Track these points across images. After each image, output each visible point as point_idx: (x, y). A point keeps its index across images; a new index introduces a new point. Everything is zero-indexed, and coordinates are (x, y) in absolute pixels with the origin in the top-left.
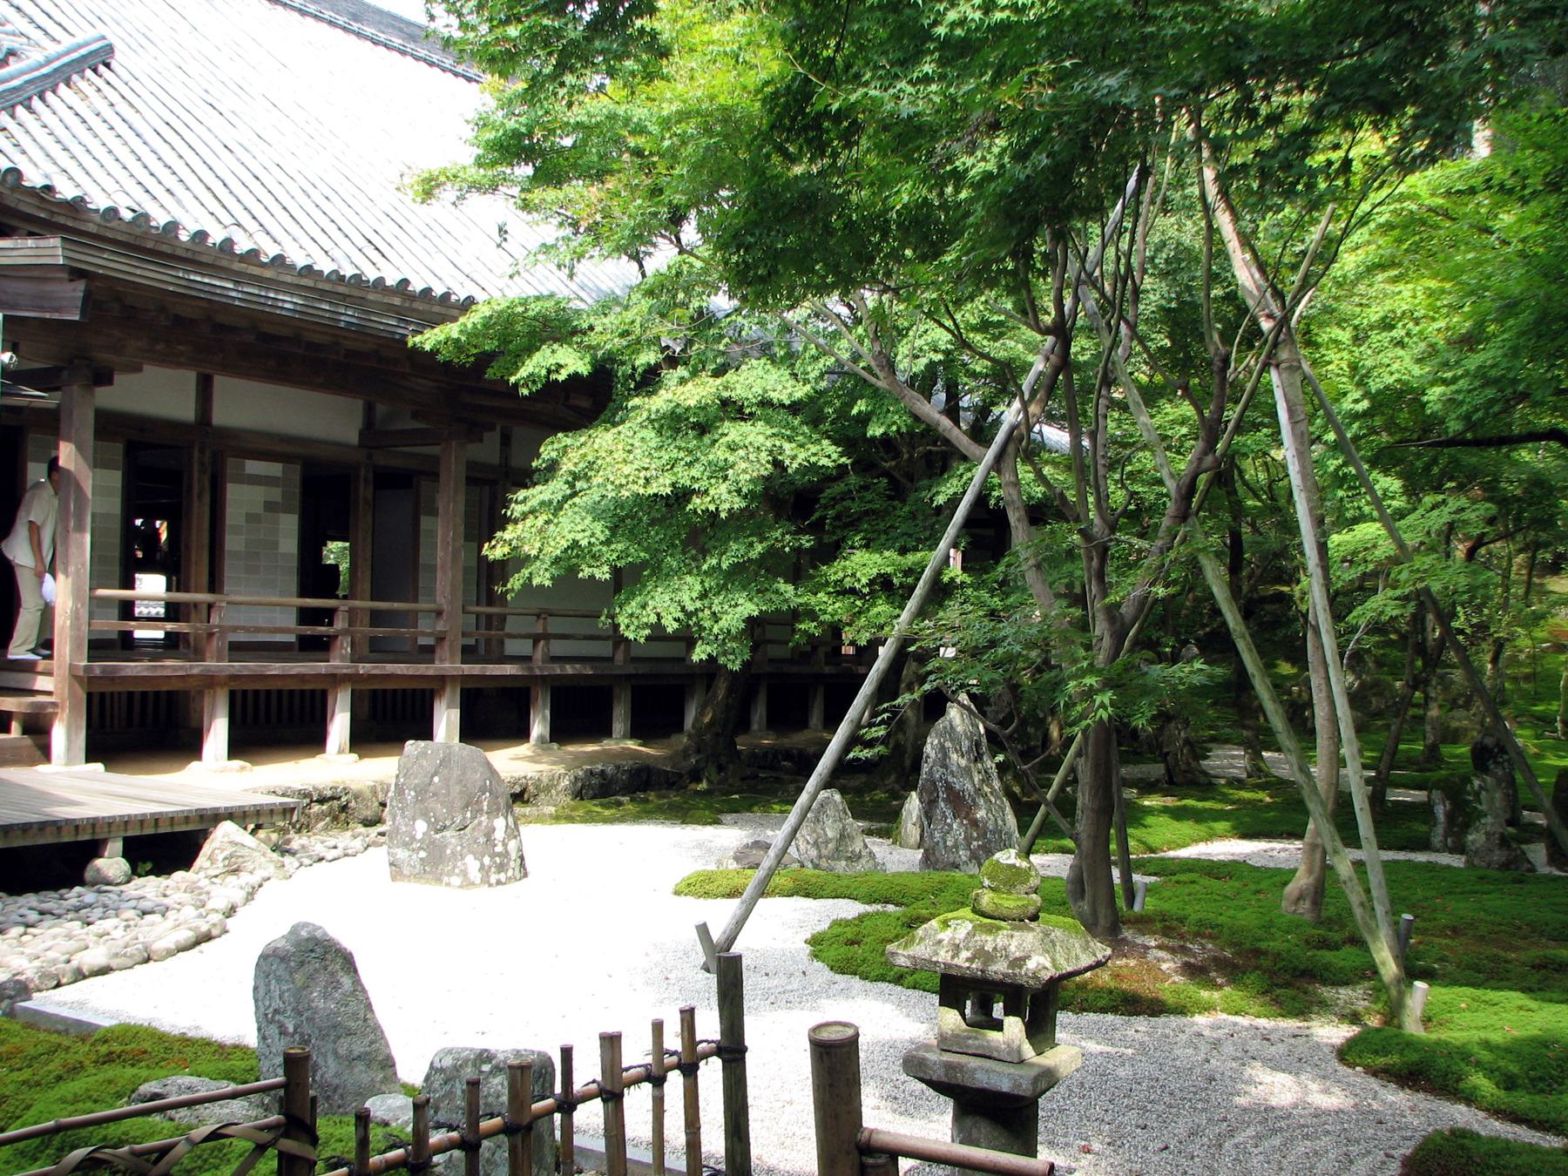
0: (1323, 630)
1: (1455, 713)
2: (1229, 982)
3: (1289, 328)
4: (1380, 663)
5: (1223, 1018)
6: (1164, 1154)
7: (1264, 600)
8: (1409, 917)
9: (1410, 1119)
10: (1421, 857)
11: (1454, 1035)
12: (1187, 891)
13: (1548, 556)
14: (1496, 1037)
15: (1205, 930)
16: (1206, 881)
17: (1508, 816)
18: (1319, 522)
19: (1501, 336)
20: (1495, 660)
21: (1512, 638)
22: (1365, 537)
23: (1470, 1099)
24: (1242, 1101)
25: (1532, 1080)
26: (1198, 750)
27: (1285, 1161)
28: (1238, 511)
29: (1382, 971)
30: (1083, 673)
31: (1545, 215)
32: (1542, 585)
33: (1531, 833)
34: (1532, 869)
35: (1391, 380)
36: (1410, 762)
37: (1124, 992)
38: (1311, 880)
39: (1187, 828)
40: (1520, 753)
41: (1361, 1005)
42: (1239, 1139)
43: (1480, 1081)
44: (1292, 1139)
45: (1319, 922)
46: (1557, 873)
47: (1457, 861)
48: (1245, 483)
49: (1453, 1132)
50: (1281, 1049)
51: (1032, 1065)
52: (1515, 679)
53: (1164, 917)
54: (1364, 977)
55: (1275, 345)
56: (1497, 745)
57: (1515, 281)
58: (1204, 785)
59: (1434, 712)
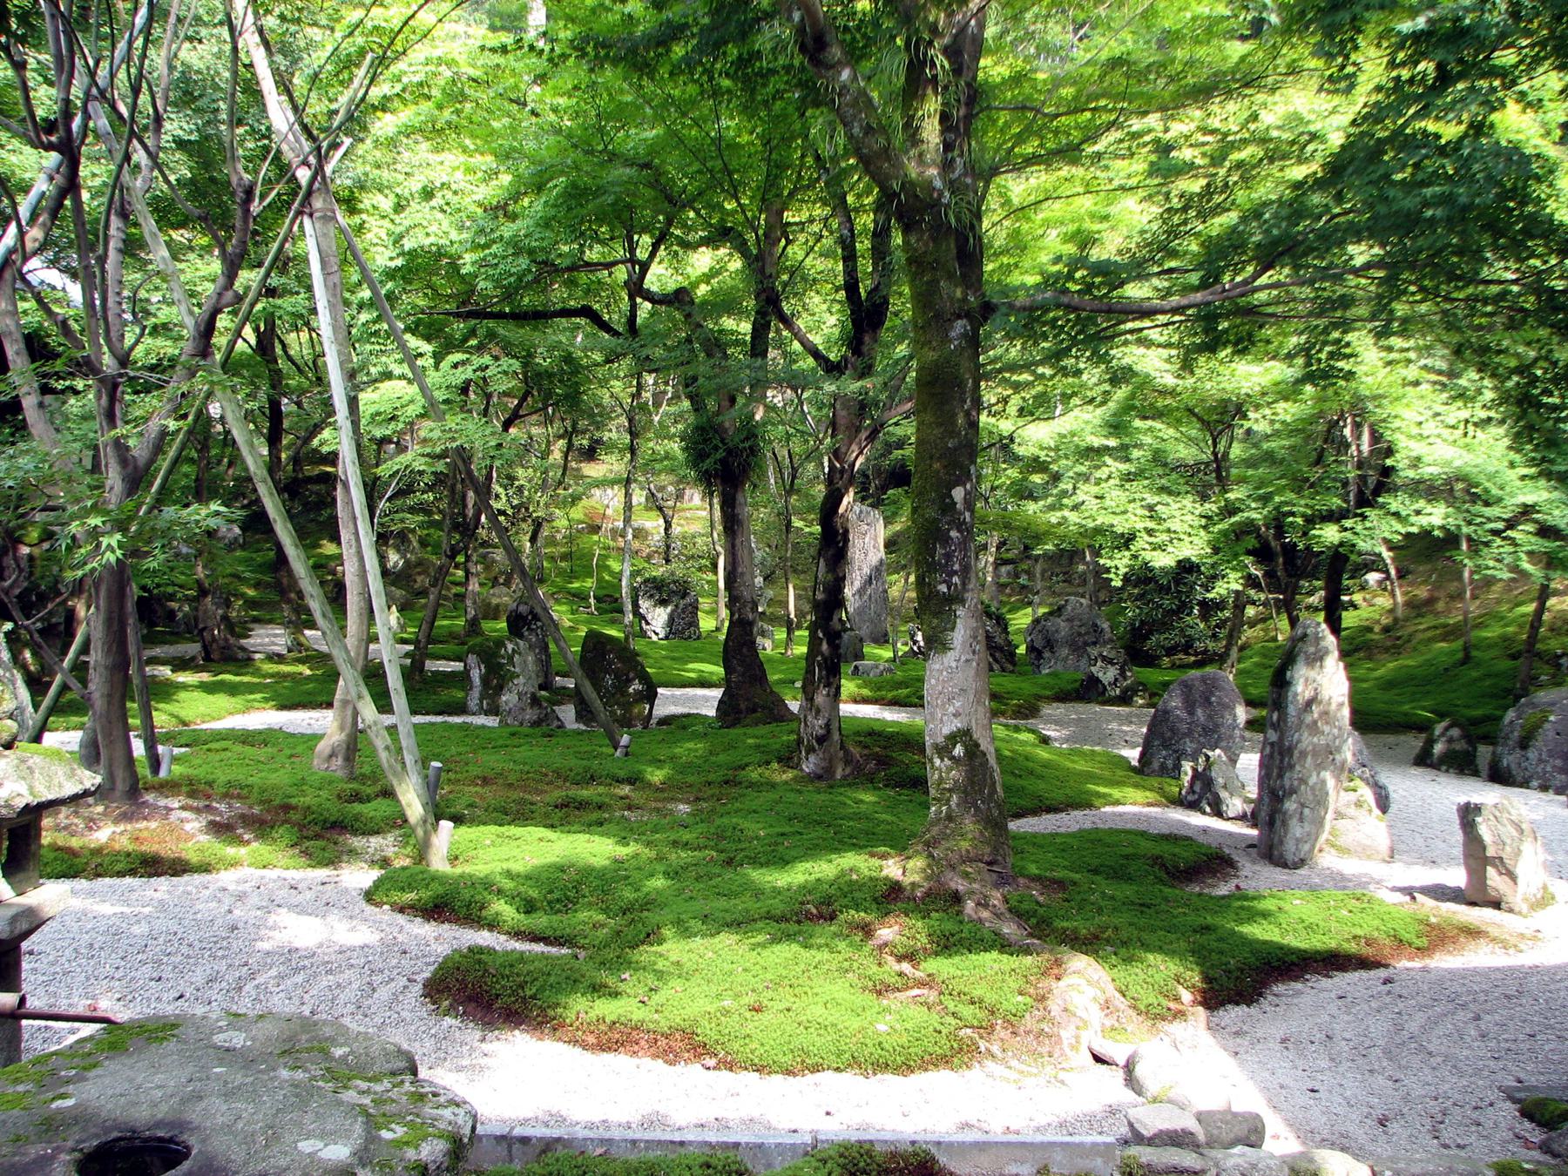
0: (352, 484)
1: (496, 590)
2: (257, 838)
3: (324, 177)
4: (423, 543)
5: (256, 873)
6: (179, 1003)
7: (310, 480)
8: (439, 764)
9: (434, 947)
10: (458, 720)
11: (478, 868)
12: (218, 757)
13: (585, 442)
14: (518, 867)
15: (233, 792)
16: (239, 748)
17: (541, 680)
18: (351, 375)
19: (533, 206)
20: (533, 539)
21: (550, 519)
22: (393, 398)
23: (492, 926)
24: (265, 946)
25: (549, 903)
26: (238, 629)
27: (307, 996)
28: (276, 379)
29: (409, 813)
30: (87, 512)
31: (576, 88)
32: (578, 470)
33: (561, 696)
34: (561, 726)
35: (427, 242)
36: (452, 636)
37: (143, 854)
38: (343, 736)
39: (221, 701)
40: (556, 625)
41: (390, 852)
42: (260, 979)
43: (504, 910)
44: (315, 974)
45: (352, 778)
46: (583, 727)
47: (491, 722)
48: (290, 358)
49: (470, 949)
50: (309, 895)
51: (10, 905)
52: (552, 559)
53: (190, 782)
54: (395, 826)
55: (309, 193)
56: (531, 612)
57: (545, 147)
58: (243, 661)
59: (474, 586)
